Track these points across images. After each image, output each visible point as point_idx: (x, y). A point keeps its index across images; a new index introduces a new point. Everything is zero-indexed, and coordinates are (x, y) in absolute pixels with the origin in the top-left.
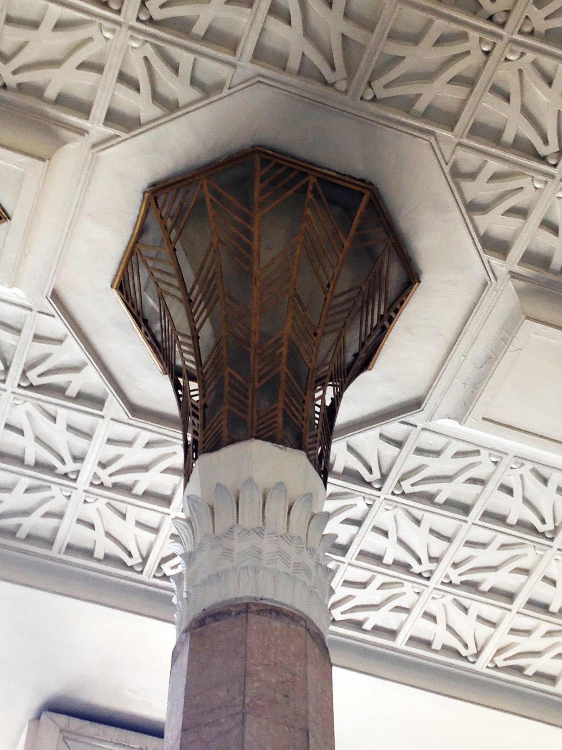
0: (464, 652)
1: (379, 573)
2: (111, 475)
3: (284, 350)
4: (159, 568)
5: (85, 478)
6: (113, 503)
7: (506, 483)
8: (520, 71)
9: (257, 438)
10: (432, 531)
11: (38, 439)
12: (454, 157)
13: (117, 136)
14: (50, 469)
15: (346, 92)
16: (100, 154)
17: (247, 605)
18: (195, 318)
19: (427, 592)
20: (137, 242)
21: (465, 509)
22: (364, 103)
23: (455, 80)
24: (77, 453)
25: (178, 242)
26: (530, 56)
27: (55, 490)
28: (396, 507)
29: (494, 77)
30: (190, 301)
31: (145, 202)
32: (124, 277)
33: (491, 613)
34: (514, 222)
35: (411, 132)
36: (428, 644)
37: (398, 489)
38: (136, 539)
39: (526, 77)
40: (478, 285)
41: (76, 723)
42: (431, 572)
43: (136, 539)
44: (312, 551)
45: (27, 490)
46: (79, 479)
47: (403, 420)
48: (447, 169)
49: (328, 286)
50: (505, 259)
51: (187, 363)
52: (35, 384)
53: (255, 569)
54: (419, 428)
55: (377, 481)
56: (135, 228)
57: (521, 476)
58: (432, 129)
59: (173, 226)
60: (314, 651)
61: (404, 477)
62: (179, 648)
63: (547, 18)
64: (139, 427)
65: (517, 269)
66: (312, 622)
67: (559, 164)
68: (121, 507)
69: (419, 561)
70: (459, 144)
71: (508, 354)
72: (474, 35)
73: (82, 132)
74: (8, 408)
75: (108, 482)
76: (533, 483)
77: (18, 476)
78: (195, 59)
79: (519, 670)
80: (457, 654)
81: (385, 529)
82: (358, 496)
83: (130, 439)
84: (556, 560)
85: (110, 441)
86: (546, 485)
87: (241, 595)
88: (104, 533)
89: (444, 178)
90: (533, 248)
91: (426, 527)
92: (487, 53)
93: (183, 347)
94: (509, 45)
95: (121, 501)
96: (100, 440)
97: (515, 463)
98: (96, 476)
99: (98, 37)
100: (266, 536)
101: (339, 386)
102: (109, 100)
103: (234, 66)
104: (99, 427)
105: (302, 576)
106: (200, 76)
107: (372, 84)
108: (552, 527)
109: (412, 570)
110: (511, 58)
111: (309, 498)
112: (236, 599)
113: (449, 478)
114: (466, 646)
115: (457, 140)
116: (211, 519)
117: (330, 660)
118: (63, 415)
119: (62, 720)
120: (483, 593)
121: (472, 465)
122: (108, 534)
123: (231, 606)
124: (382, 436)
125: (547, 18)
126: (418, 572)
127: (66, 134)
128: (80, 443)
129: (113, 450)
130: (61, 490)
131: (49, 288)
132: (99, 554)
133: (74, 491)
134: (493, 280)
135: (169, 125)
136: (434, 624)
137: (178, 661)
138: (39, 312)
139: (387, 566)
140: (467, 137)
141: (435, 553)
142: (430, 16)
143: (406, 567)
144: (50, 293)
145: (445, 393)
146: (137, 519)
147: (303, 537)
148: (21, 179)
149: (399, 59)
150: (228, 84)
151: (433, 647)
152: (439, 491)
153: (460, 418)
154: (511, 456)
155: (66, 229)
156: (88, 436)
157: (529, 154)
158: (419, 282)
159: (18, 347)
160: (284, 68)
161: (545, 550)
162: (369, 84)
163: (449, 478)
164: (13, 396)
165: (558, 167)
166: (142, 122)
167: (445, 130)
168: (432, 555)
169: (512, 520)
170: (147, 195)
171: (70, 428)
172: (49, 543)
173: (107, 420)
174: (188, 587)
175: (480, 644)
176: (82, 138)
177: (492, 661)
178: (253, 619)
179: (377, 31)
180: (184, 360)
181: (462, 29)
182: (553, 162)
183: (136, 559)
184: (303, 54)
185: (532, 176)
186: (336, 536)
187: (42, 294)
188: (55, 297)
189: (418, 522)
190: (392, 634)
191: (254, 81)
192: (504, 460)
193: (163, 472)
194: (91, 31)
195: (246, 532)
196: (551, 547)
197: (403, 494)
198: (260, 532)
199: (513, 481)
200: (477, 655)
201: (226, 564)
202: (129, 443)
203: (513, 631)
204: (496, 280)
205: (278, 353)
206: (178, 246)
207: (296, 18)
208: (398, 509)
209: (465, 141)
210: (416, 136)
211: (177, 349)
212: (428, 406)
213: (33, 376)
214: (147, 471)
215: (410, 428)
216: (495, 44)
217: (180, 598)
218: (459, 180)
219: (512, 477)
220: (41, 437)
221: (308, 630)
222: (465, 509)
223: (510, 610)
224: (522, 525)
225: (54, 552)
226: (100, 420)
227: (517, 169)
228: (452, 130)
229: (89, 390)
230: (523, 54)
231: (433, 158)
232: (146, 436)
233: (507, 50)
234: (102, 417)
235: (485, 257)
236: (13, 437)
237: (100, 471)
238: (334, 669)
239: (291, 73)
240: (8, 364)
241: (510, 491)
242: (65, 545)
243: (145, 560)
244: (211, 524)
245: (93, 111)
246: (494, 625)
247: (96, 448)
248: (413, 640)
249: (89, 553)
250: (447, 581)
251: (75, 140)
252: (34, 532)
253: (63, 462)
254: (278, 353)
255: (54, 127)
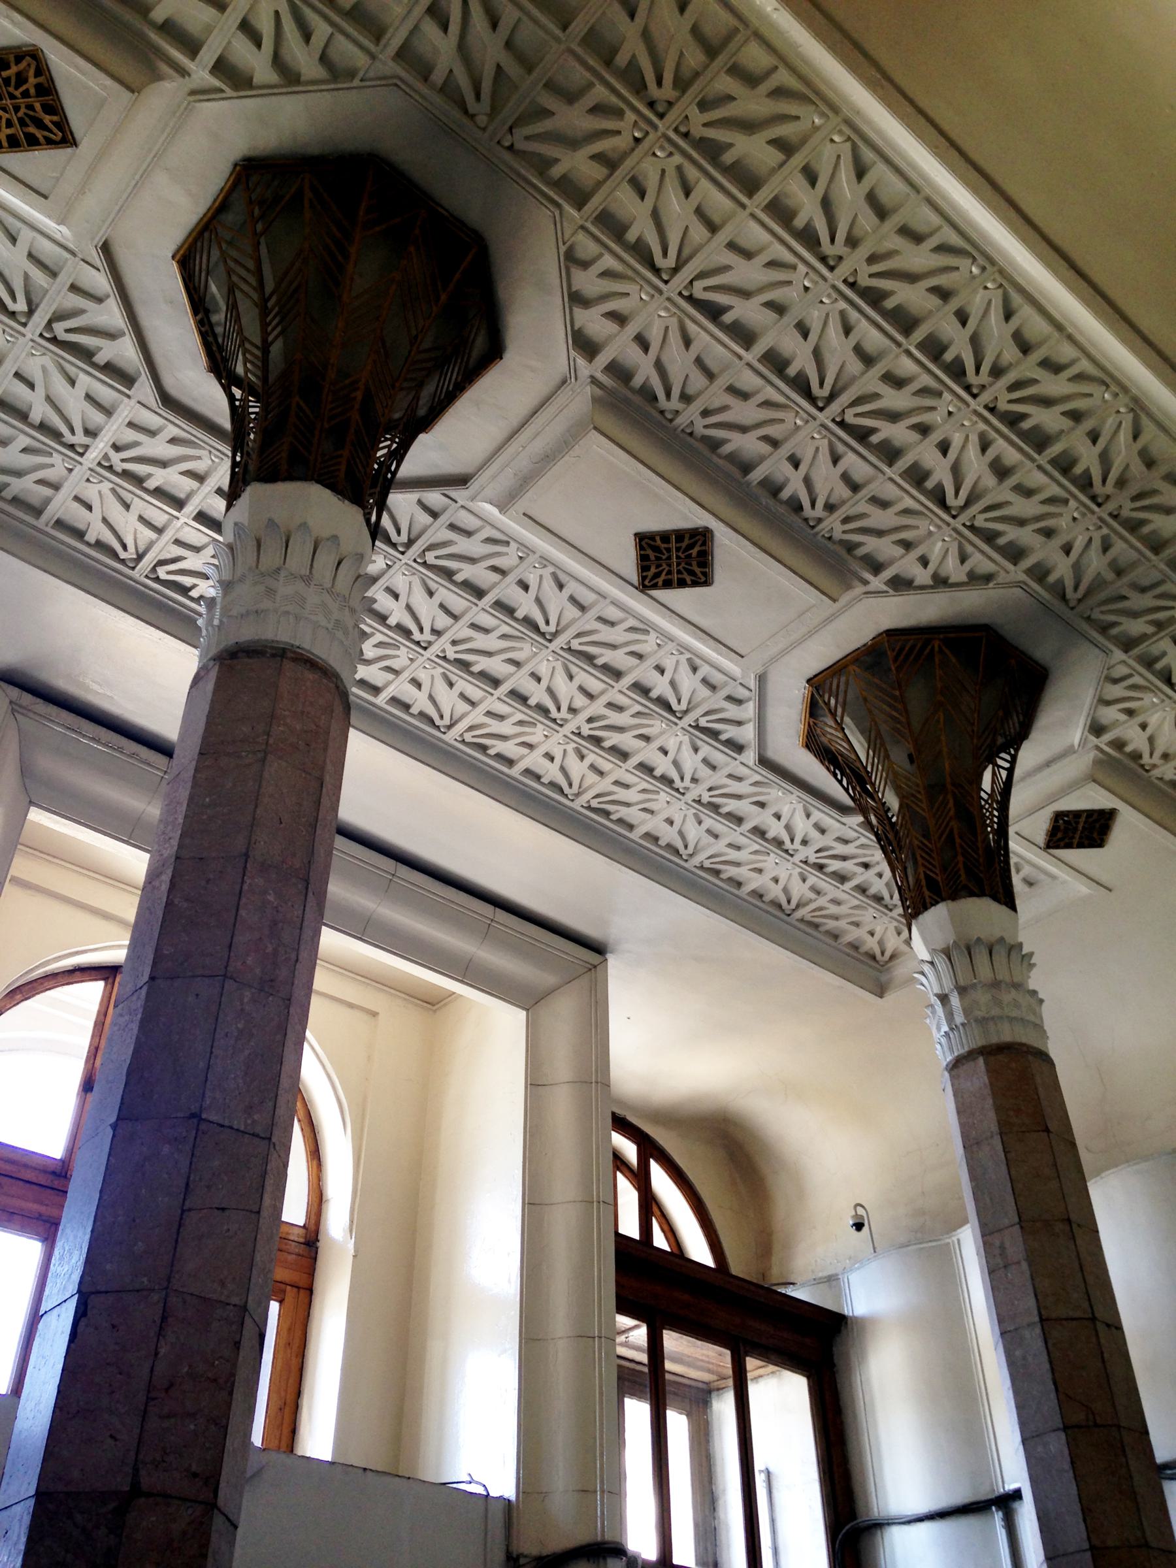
0: (438, 722)
1: (520, 711)
2: (123, 460)
3: (359, 395)
4: (154, 569)
5: (93, 455)
6: (119, 490)
7: (525, 580)
8: (663, 171)
9: (318, 482)
10: (442, 606)
11: (49, 399)
12: (573, 239)
13: (222, 91)
14: (56, 435)
15: (484, 129)
16: (198, 105)
17: (284, 649)
18: (270, 329)
19: (421, 660)
20: (213, 217)
21: (479, 593)
22: (498, 148)
23: (598, 157)
24: (91, 427)
25: (263, 237)
26: (677, 159)
27: (56, 459)
28: (414, 574)
29: (635, 170)
30: (266, 307)
31: (233, 176)
32: (190, 252)
33: (474, 693)
34: (611, 327)
35: (538, 197)
36: (406, 707)
37: (421, 558)
38: (135, 534)
39: (667, 179)
40: (557, 379)
41: (27, 699)
42: (566, 721)
43: (135, 534)
44: (353, 611)
45: (25, 450)
46: (87, 454)
47: (446, 492)
48: (563, 249)
49: (416, 336)
50: (590, 362)
51: (249, 375)
52: (59, 338)
53: (297, 618)
54: (458, 505)
55: (403, 544)
56: (215, 200)
57: (541, 577)
58: (561, 201)
59: (262, 217)
60: (338, 709)
61: (431, 547)
62: (202, 674)
63: (705, 125)
64: (166, 419)
65: (599, 376)
66: (342, 680)
67: (671, 282)
68: (128, 497)
69: (421, 630)
70: (582, 227)
71: (566, 458)
72: (630, 116)
73: (183, 72)
74: (24, 354)
75: (119, 467)
76: (549, 586)
77: (17, 432)
78: (332, 34)
79: (483, 748)
80: (431, 721)
81: (398, 592)
82: (380, 553)
83: (153, 428)
84: (548, 660)
85: (131, 425)
86: (561, 591)
87: (278, 638)
88: (101, 518)
89: (556, 258)
90: (620, 359)
91: (437, 599)
92: (637, 140)
93: (248, 356)
94: (662, 140)
95: (130, 492)
96: (120, 420)
97: (539, 563)
98: (106, 457)
99: (635, 296)
100: (312, 586)
101: (988, 826)
102: (224, 44)
103: (373, 57)
104: (122, 406)
105: (339, 634)
106: (333, 53)
107: (514, 131)
108: (553, 630)
109: (412, 637)
110: (659, 154)
111: (360, 558)
112: (273, 641)
113: (472, 560)
114: (442, 717)
115: (581, 222)
116: (255, 554)
117: (349, 719)
118: (84, 380)
119: (14, 692)
120: (471, 674)
121: (637, 641)
122: (105, 520)
123: (266, 646)
124: (420, 502)
125: (705, 125)
126: (417, 640)
127: (164, 68)
128: (97, 417)
129: (131, 435)
130: (63, 460)
131: (101, 238)
132: (91, 537)
133: (79, 466)
134: (573, 379)
135: (284, 99)
136: (417, 691)
137: (201, 684)
138: (83, 260)
139: (389, 627)
140: (592, 223)
141: (439, 626)
142: (593, 79)
143: (407, 633)
144: (101, 243)
145: (494, 477)
146: (142, 513)
147: (347, 596)
148: (101, 104)
149: (547, 113)
150: (361, 74)
151: (411, 711)
152: (461, 570)
153: (502, 507)
154: (537, 556)
155: (137, 177)
156: (108, 412)
157: (455, 102)
158: (501, 358)
159: (50, 292)
160: (426, 79)
161: (17, 338)
162: (511, 129)
163: (472, 560)
164: (31, 344)
165: (669, 284)
166: (254, 84)
167: (572, 206)
168: (435, 628)
169: (520, 614)
170: (238, 168)
171: (89, 397)
172: (38, 512)
173: (133, 402)
174: (221, 615)
175: (455, 718)
176: (181, 79)
177: (461, 735)
178: (288, 665)
179: (535, 74)
180: (247, 370)
181: (623, 106)
182: (665, 277)
183: (130, 554)
184: (451, 71)
185: (797, 412)
186: (375, 601)
187: (93, 239)
188: (106, 249)
189: (431, 594)
190: (510, 762)
191: (391, 81)
192: (530, 557)
193: (181, 473)
194: (788, 416)
195: (293, 576)
196: (547, 647)
197: (425, 564)
198: (307, 579)
199: (532, 580)
200: (450, 727)
201: (266, 604)
202: (152, 433)
203: (489, 714)
204: (576, 379)
205: (353, 395)
206: (262, 240)
207: (454, 27)
208: (559, 662)
209: (589, 225)
210: (542, 203)
211: (240, 357)
212: (474, 486)
213: (59, 328)
214: (165, 468)
215: (450, 502)
216: (647, 133)
217: (209, 622)
218: (570, 264)
219: (532, 575)
220: (52, 397)
221: (337, 687)
222: (479, 593)
223: (492, 695)
224: (529, 622)
225: (41, 523)
226: (126, 400)
227: (630, 273)
228: (579, 210)
229: (121, 364)
230: (671, 154)
231: (553, 232)
232: (173, 431)
233: (658, 145)
234: (129, 397)
235: (573, 353)
236: (20, 389)
237: (112, 453)
238: (351, 730)
239: (432, 87)
240: (34, 307)
241: (525, 587)
242: (55, 519)
243: (140, 557)
244: (255, 558)
245: (202, 53)
246: (473, 704)
247: (115, 427)
248: (394, 701)
249: (80, 534)
250: (577, 731)
251: (171, 79)
252: (22, 496)
253: (73, 432)
254: (353, 395)
255: (152, 56)
